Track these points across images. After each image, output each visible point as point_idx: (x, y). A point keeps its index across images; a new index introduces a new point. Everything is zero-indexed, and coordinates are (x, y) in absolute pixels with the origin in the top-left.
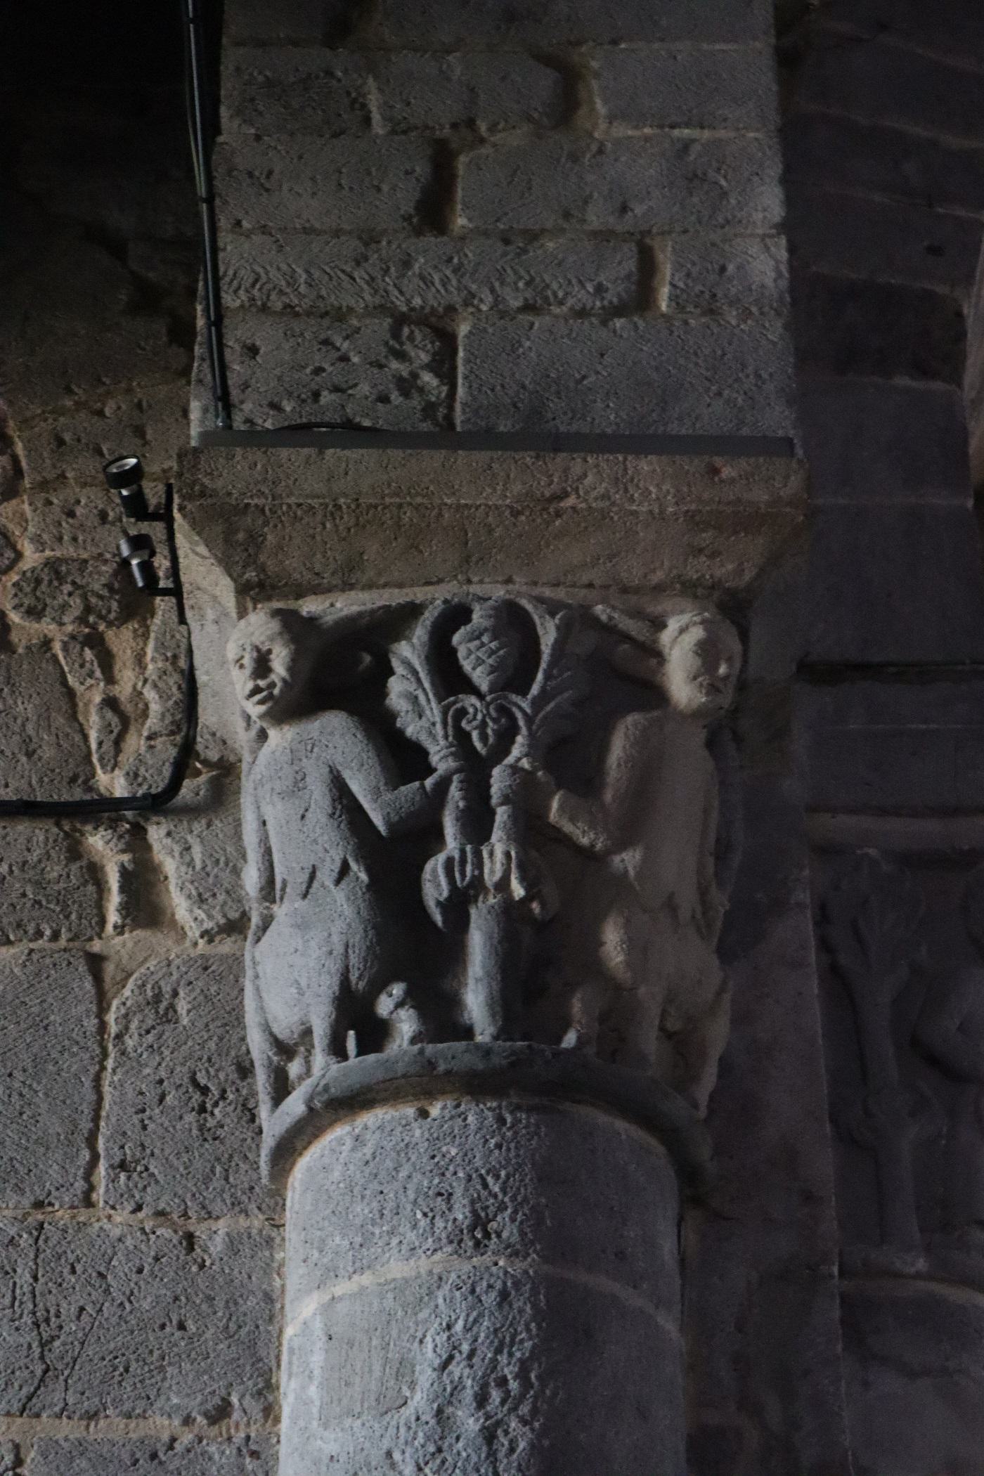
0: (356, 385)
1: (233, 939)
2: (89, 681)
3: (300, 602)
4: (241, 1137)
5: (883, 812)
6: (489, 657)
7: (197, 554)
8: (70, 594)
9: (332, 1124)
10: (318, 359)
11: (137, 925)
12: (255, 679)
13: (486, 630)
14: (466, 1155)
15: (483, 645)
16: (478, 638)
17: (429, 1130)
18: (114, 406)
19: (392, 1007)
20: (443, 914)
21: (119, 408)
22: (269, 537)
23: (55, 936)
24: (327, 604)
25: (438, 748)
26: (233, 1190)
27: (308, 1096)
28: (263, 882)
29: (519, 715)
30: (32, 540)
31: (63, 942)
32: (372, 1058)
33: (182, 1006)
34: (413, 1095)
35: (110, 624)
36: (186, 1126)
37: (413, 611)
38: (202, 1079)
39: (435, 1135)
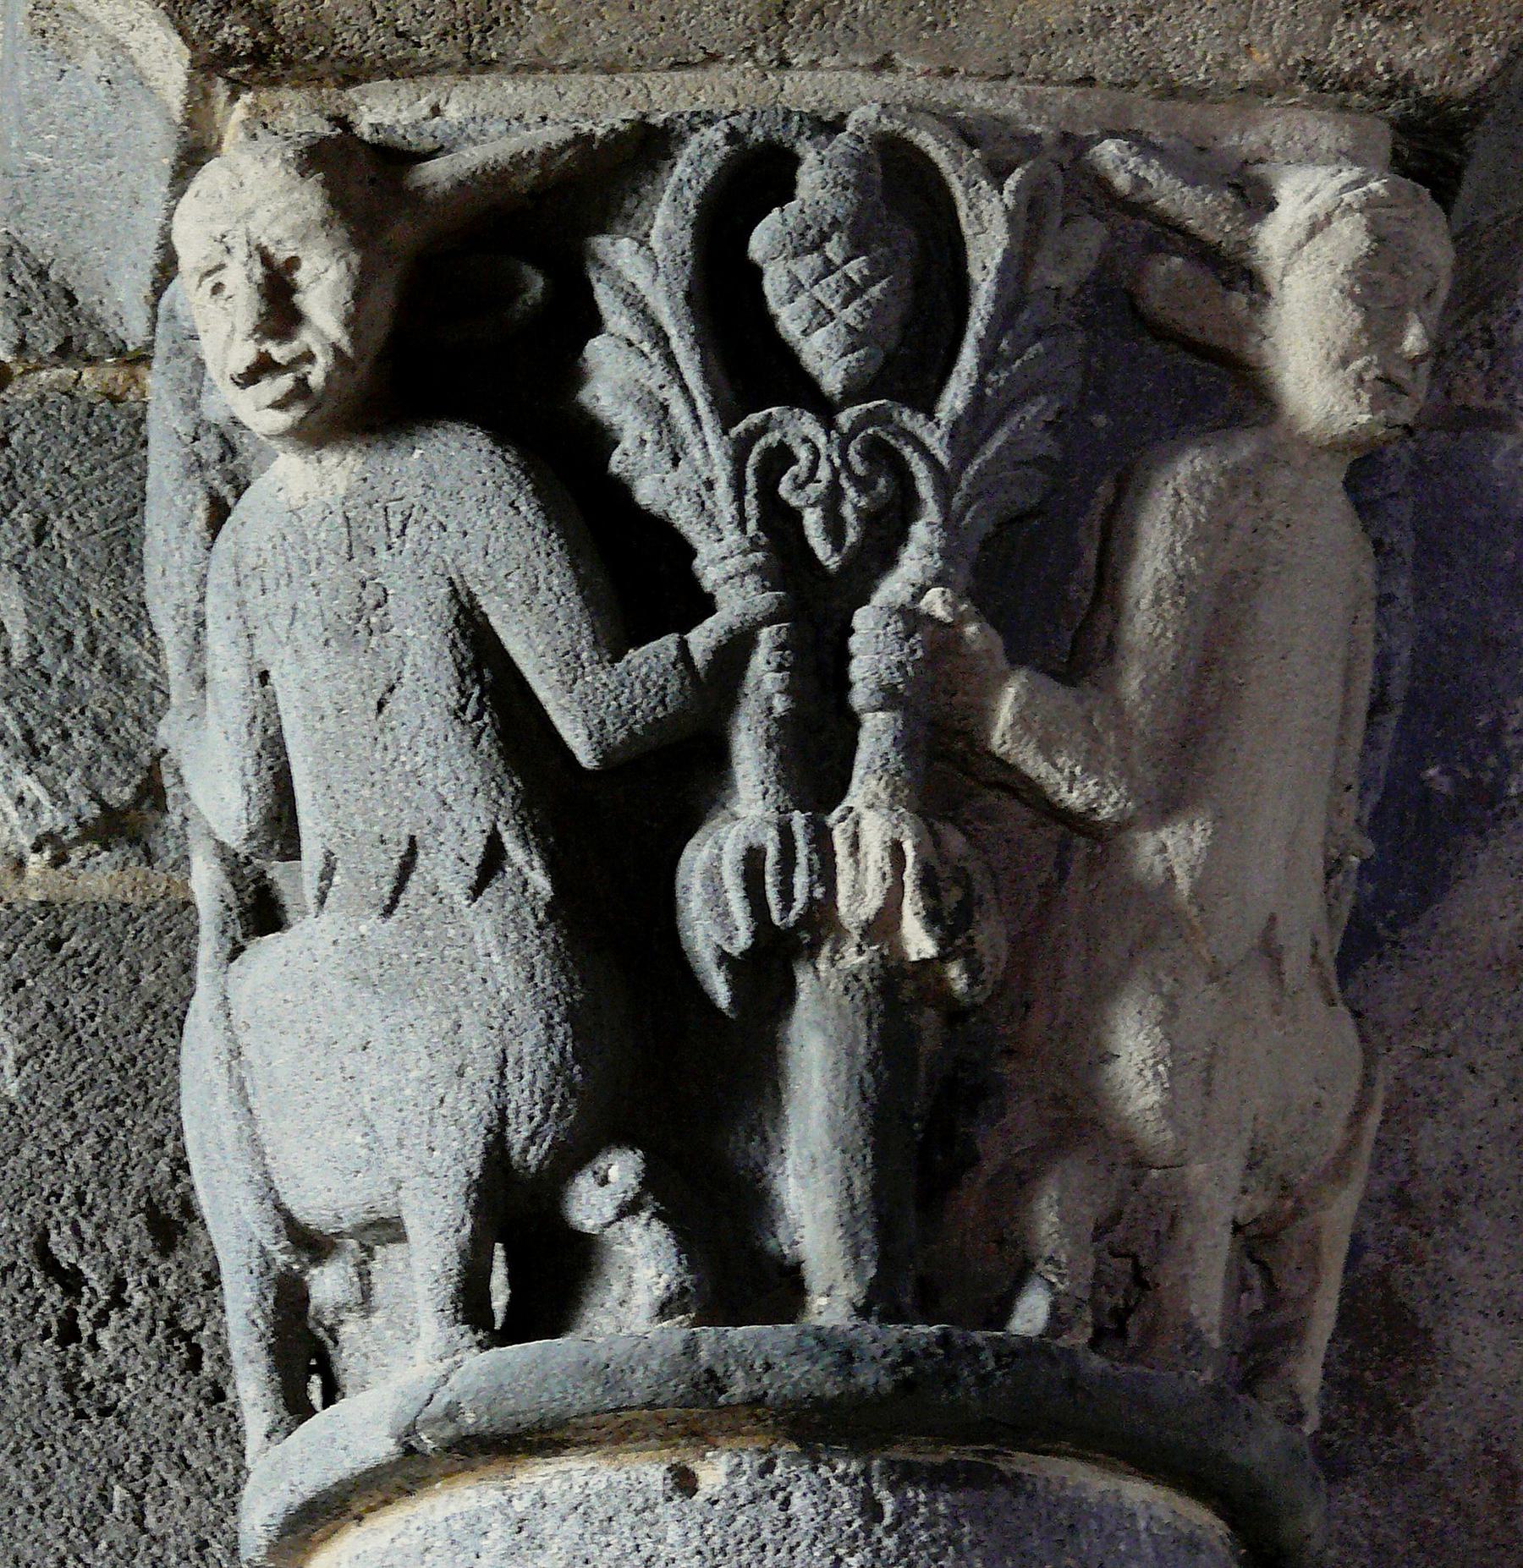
1: (117, 855)
3: (352, 93)
4: (169, 1408)
6: (845, 304)
12: (259, 341)
15: (829, 268)
16: (817, 247)
19: (609, 1213)
20: (733, 985)
25: (720, 550)
26: (156, 1550)
28: (256, 817)
29: (919, 469)
34: (660, 1437)
36: (33, 1378)
39: (716, 1541)
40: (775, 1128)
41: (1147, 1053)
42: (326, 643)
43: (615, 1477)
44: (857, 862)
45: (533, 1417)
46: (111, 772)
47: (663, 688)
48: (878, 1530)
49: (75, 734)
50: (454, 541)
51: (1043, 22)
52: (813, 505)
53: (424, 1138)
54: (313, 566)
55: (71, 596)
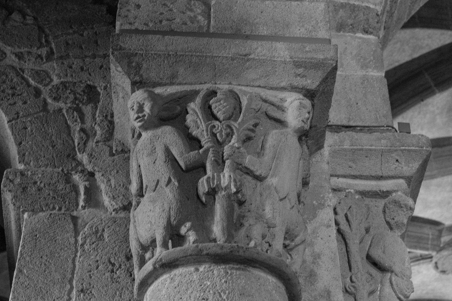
0: (175, 19)
1: (125, 212)
2: (75, 123)
3: (154, 89)
5: (355, 177)
6: (223, 108)
7: (117, 71)
8: (69, 93)
9: (162, 274)
10: (162, 10)
11: (90, 207)
13: (222, 99)
18: (87, 33)
19: (186, 231)
21: (89, 33)
22: (144, 65)
23: (60, 209)
24: (164, 90)
25: (204, 139)
27: (154, 263)
28: (138, 187)
29: (234, 129)
30: (56, 75)
31: (63, 211)
32: (179, 248)
33: (106, 235)
35: (83, 104)
37: (196, 93)
38: (112, 260)
39: (202, 278)
43: (186, 270)
48: (227, 276)
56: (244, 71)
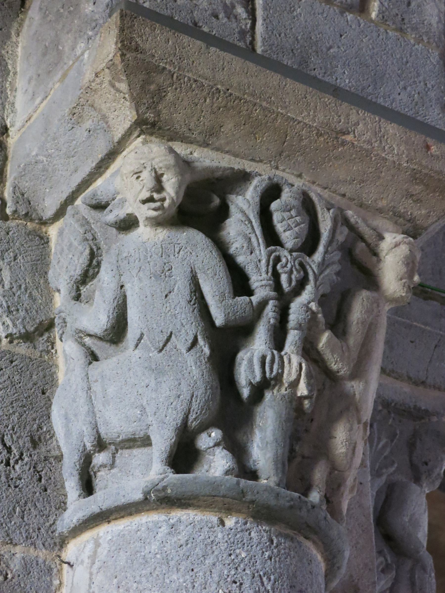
1: (27, 345)
6: (296, 227)
12: (152, 192)
13: (294, 207)
14: (251, 559)
17: (228, 535)
24: (188, 151)
28: (109, 325)
39: (232, 540)
40: (251, 434)
41: (344, 438)
42: (151, 278)
44: (290, 366)
45: (190, 494)
46: (29, 322)
47: (245, 308)
48: (273, 547)
49: (20, 311)
50: (194, 258)
51: (339, 177)
52: (286, 273)
53: (164, 413)
54: (149, 257)
55: (22, 276)
56: (330, 160)
